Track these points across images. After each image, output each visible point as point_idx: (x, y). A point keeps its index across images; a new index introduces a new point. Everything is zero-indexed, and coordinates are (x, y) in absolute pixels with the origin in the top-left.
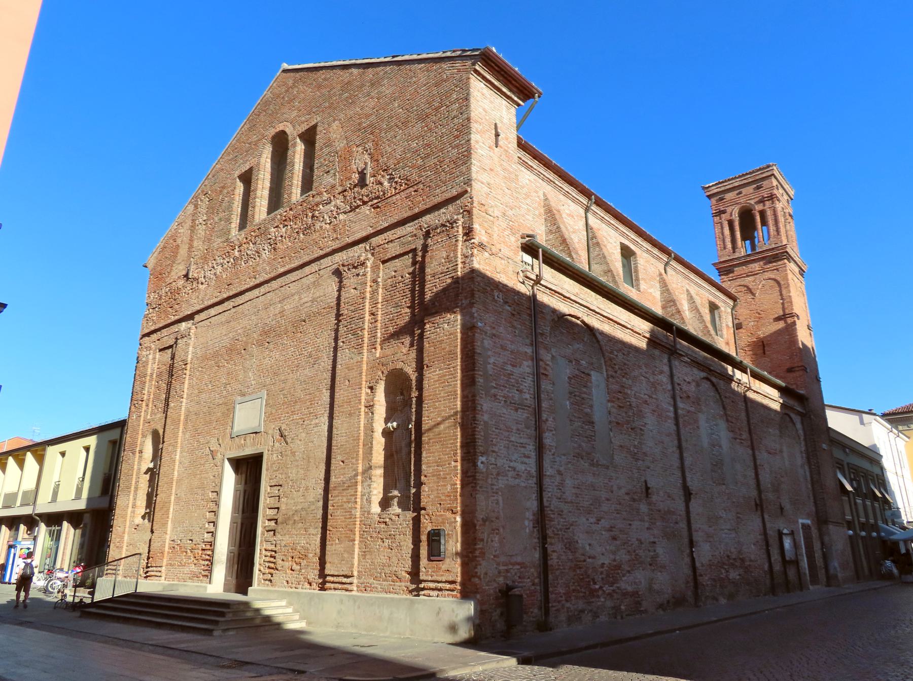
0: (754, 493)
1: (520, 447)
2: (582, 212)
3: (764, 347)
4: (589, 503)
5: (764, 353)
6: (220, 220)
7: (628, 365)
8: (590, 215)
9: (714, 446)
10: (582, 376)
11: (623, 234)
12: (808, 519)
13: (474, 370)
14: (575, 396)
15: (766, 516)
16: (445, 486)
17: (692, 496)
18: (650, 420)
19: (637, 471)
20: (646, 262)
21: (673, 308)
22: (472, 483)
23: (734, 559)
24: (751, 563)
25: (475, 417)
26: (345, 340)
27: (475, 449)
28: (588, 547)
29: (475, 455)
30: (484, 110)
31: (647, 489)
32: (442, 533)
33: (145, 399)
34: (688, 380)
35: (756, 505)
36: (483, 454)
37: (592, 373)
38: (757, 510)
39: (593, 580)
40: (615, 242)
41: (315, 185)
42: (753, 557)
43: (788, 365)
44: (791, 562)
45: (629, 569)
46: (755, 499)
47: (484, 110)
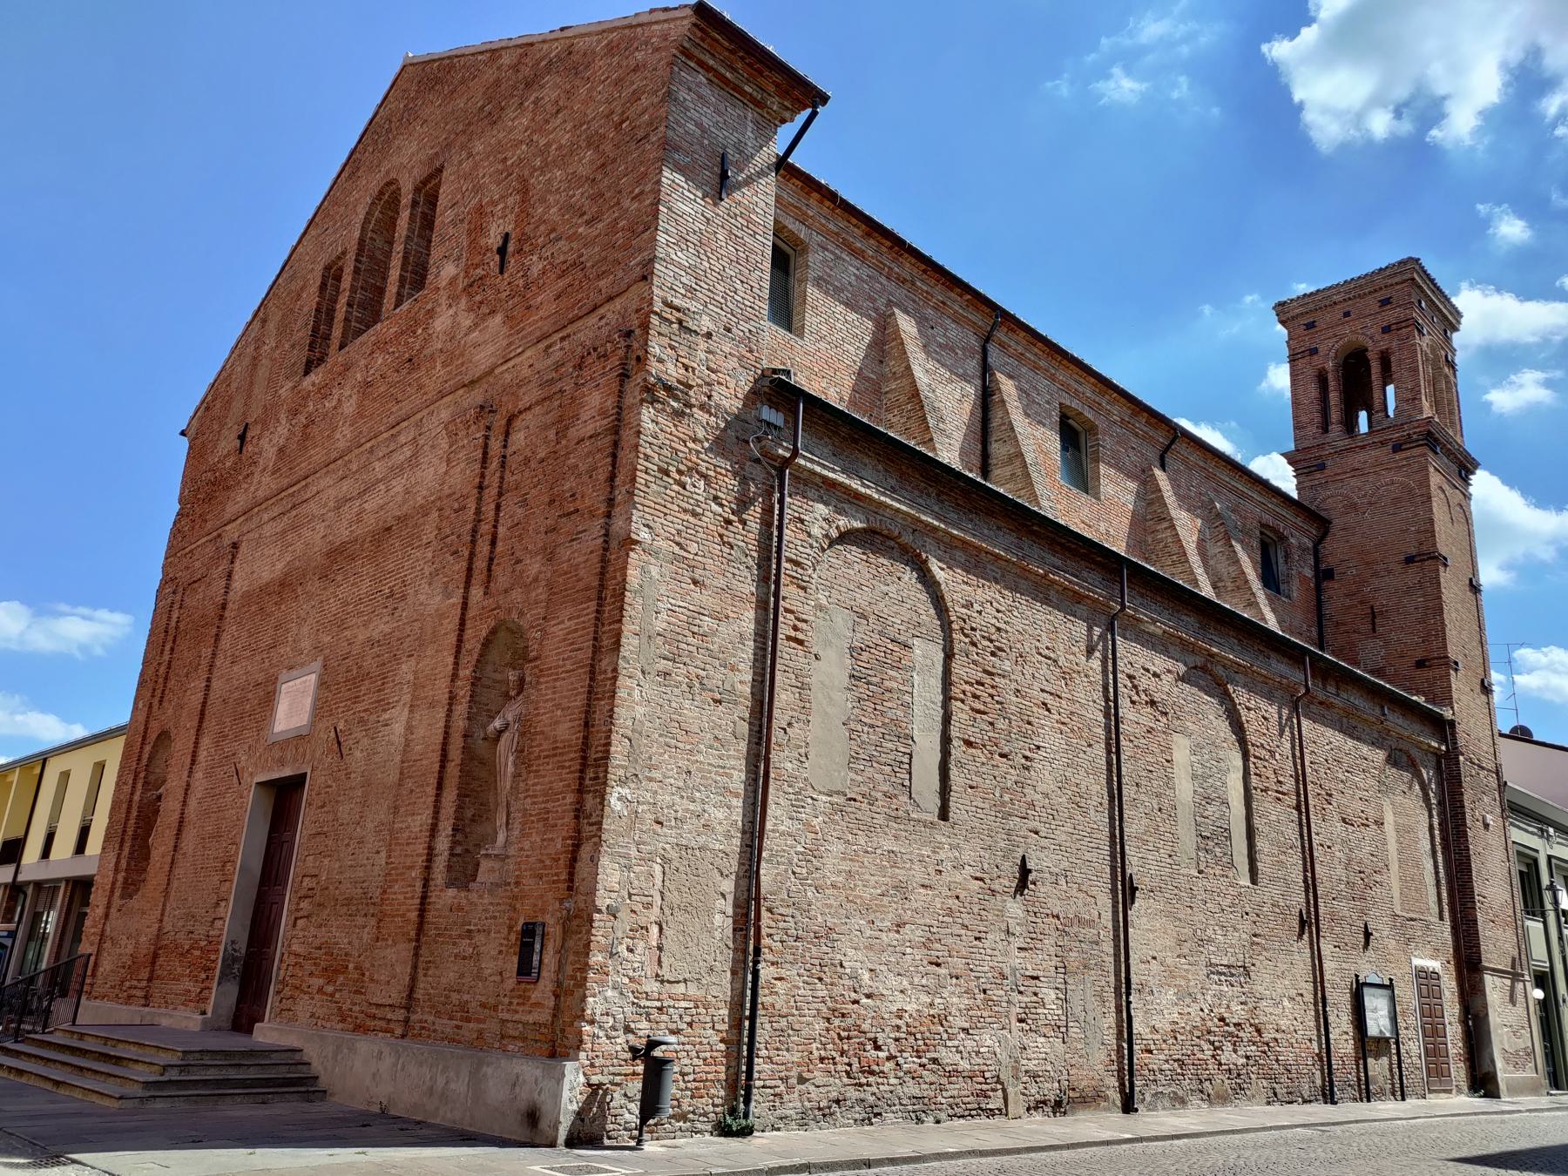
0: (1298, 899)
1: (717, 773)
2: (975, 343)
3: (1374, 617)
4: (879, 891)
5: (1374, 630)
6: (293, 346)
7: (1007, 632)
8: (991, 348)
9: (1208, 800)
10: (890, 646)
11: (1066, 388)
12: (1433, 957)
13: (620, 621)
14: (868, 683)
15: (1327, 948)
16: (552, 840)
17: (1137, 893)
18: (1050, 737)
19: (1005, 837)
20: (1118, 443)
21: (1168, 533)
22: (594, 836)
23: (1237, 1025)
24: (1278, 1036)
25: (612, 710)
26: (731, 614)
27: (606, 772)
28: (866, 976)
29: (605, 784)
30: (699, 125)
31: (1024, 871)
32: (539, 931)
33: (687, 766)
34: (1152, 668)
35: (1302, 923)
36: (622, 782)
37: (916, 641)
38: (1300, 936)
39: (875, 1041)
40: (1048, 403)
41: (430, 277)
42: (1284, 1023)
43: (1419, 655)
44: (1381, 1041)
45: (966, 1025)
46: (1301, 911)
47: (699, 125)
